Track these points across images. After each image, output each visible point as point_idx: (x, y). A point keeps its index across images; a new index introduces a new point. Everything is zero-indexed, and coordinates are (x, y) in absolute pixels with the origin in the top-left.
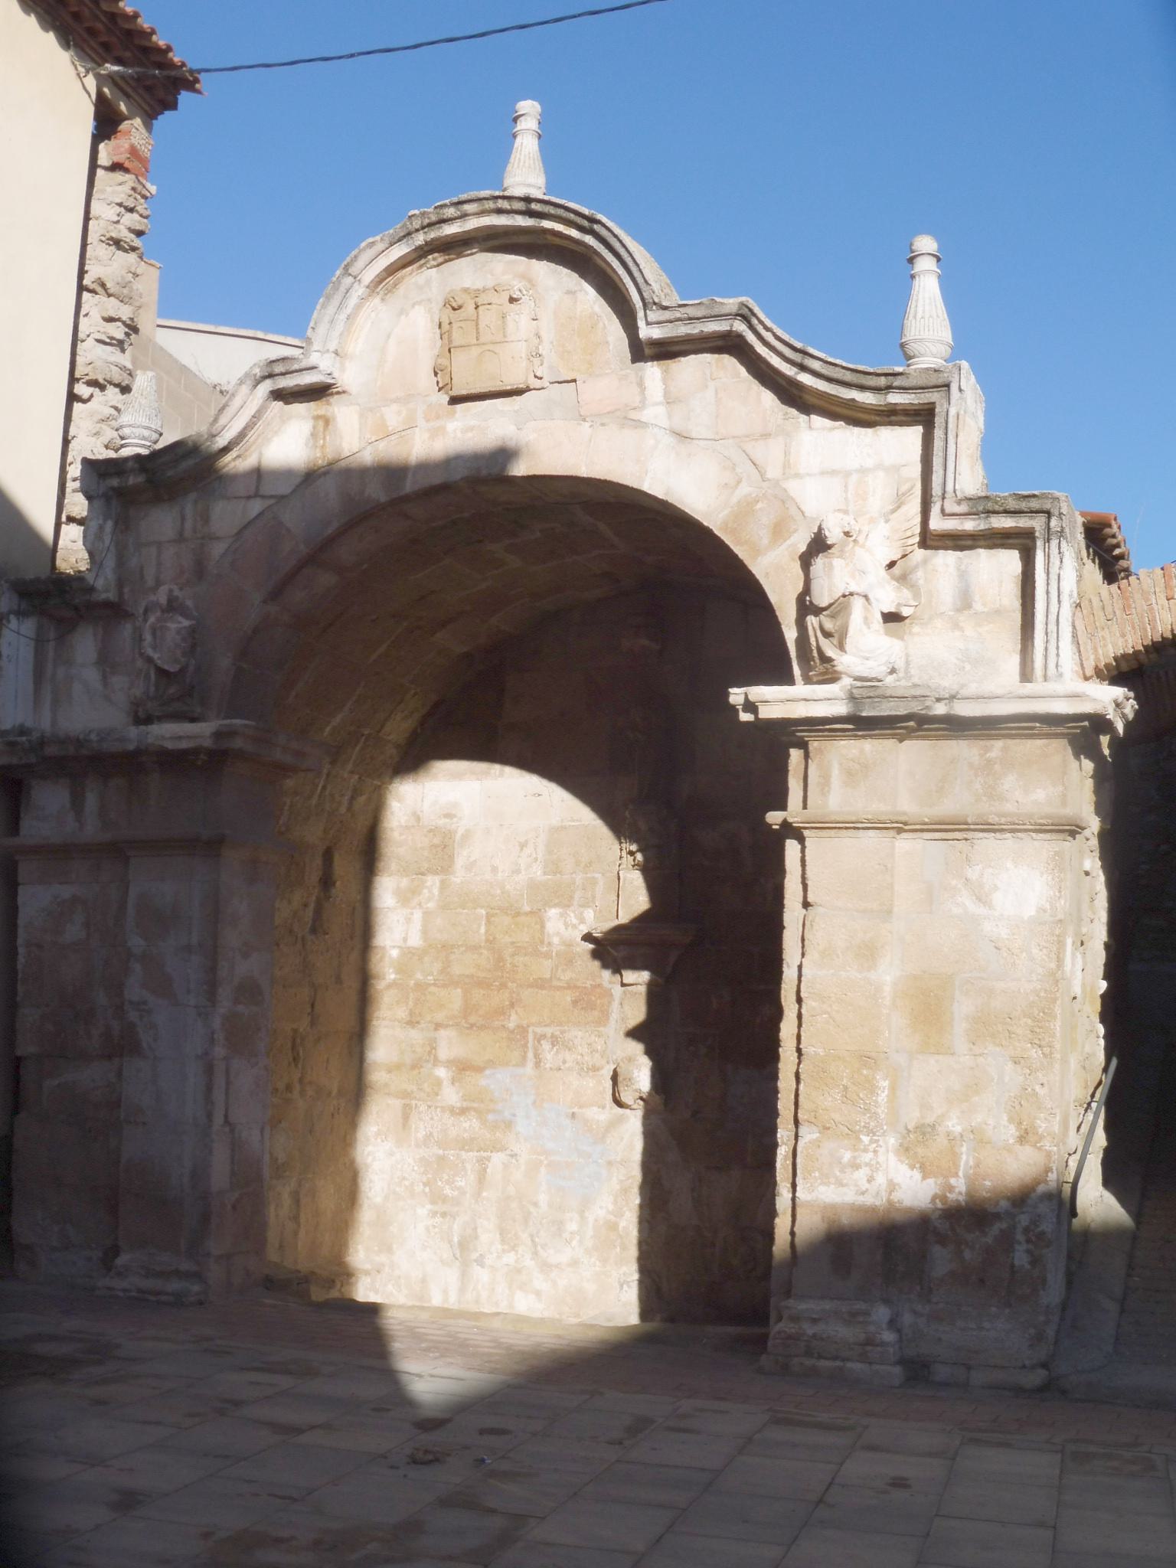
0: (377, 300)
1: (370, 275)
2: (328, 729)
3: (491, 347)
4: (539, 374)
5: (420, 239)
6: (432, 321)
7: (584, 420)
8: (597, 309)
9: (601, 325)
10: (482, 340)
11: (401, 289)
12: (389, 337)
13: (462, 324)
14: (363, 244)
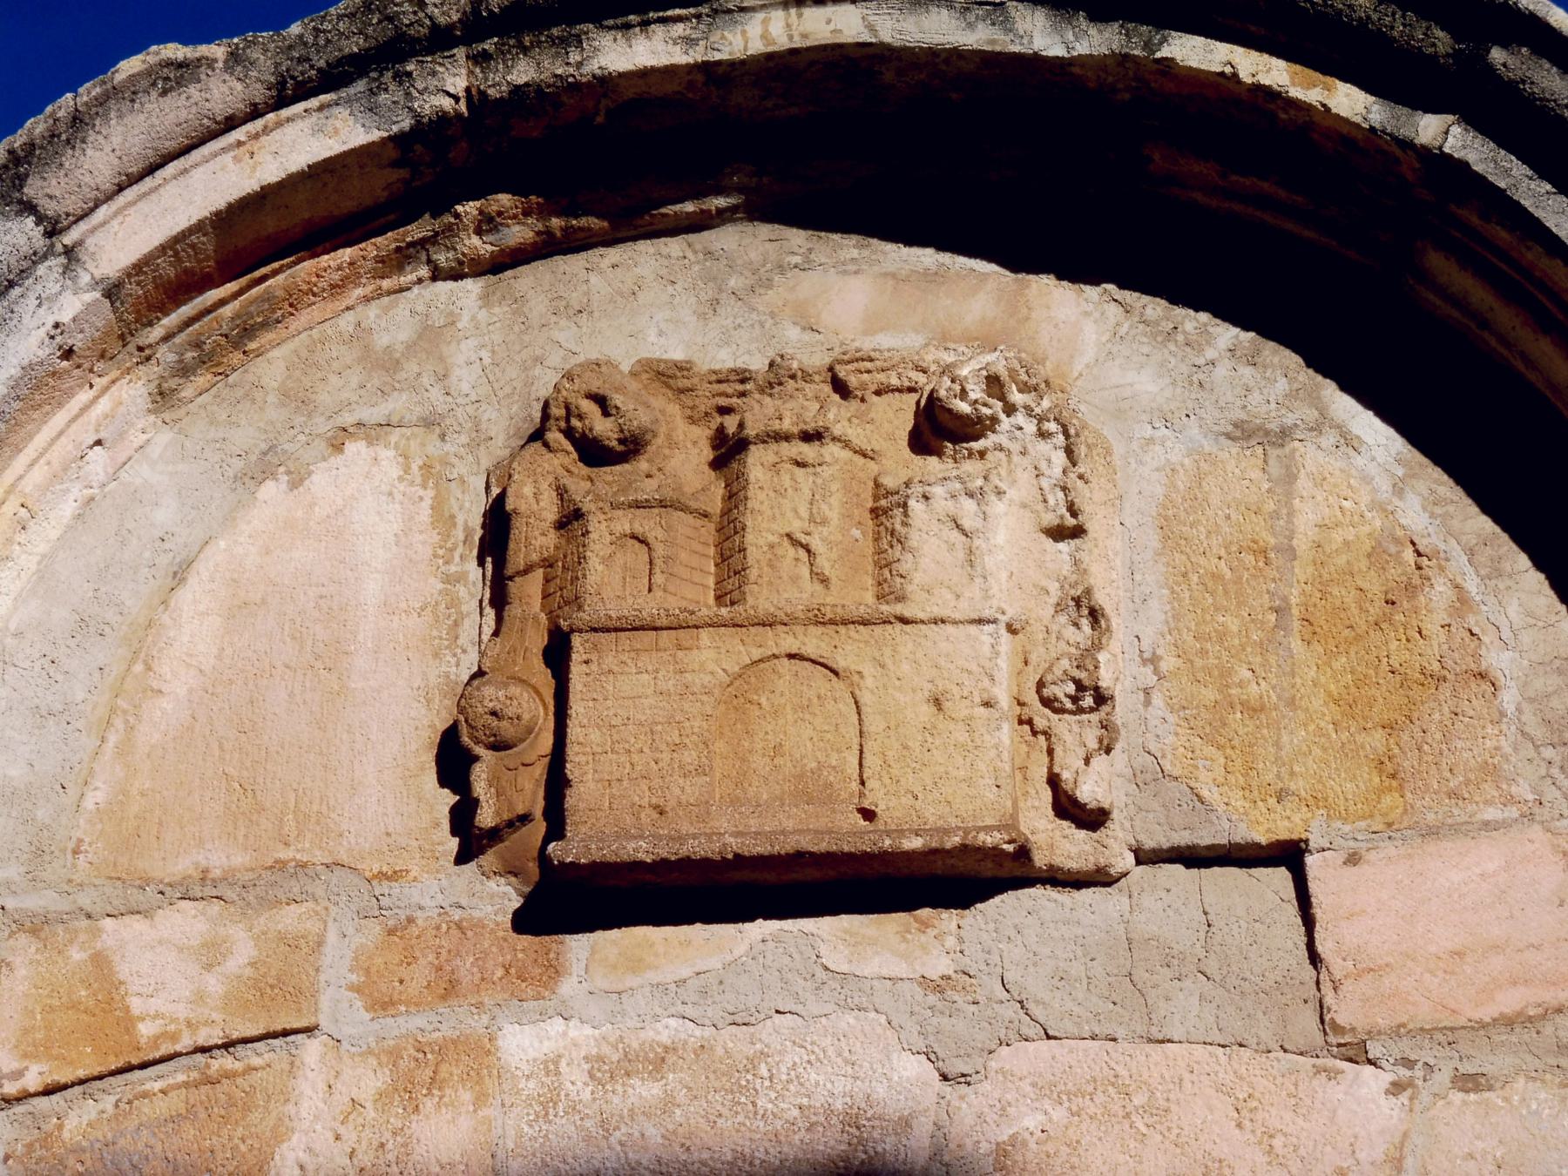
0: (132, 391)
1: (128, 236)
2: (1306, 233)
3: (813, 642)
4: (1088, 792)
5: (447, 85)
6: (443, 519)
7: (1357, 1054)
8: (1414, 516)
9: (1440, 592)
10: (760, 599)
11: (274, 362)
12: (179, 576)
13: (646, 523)
14: (130, 66)
